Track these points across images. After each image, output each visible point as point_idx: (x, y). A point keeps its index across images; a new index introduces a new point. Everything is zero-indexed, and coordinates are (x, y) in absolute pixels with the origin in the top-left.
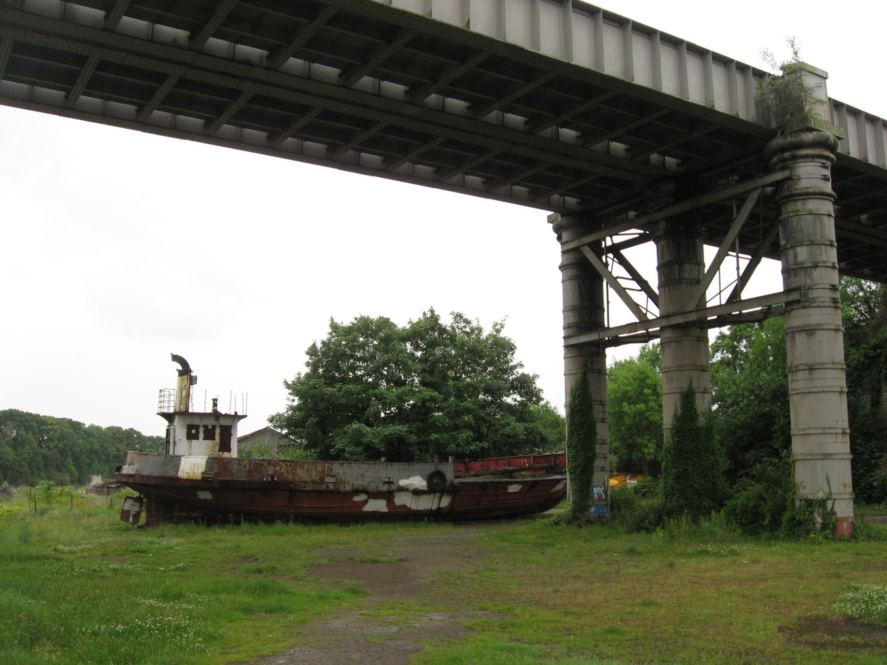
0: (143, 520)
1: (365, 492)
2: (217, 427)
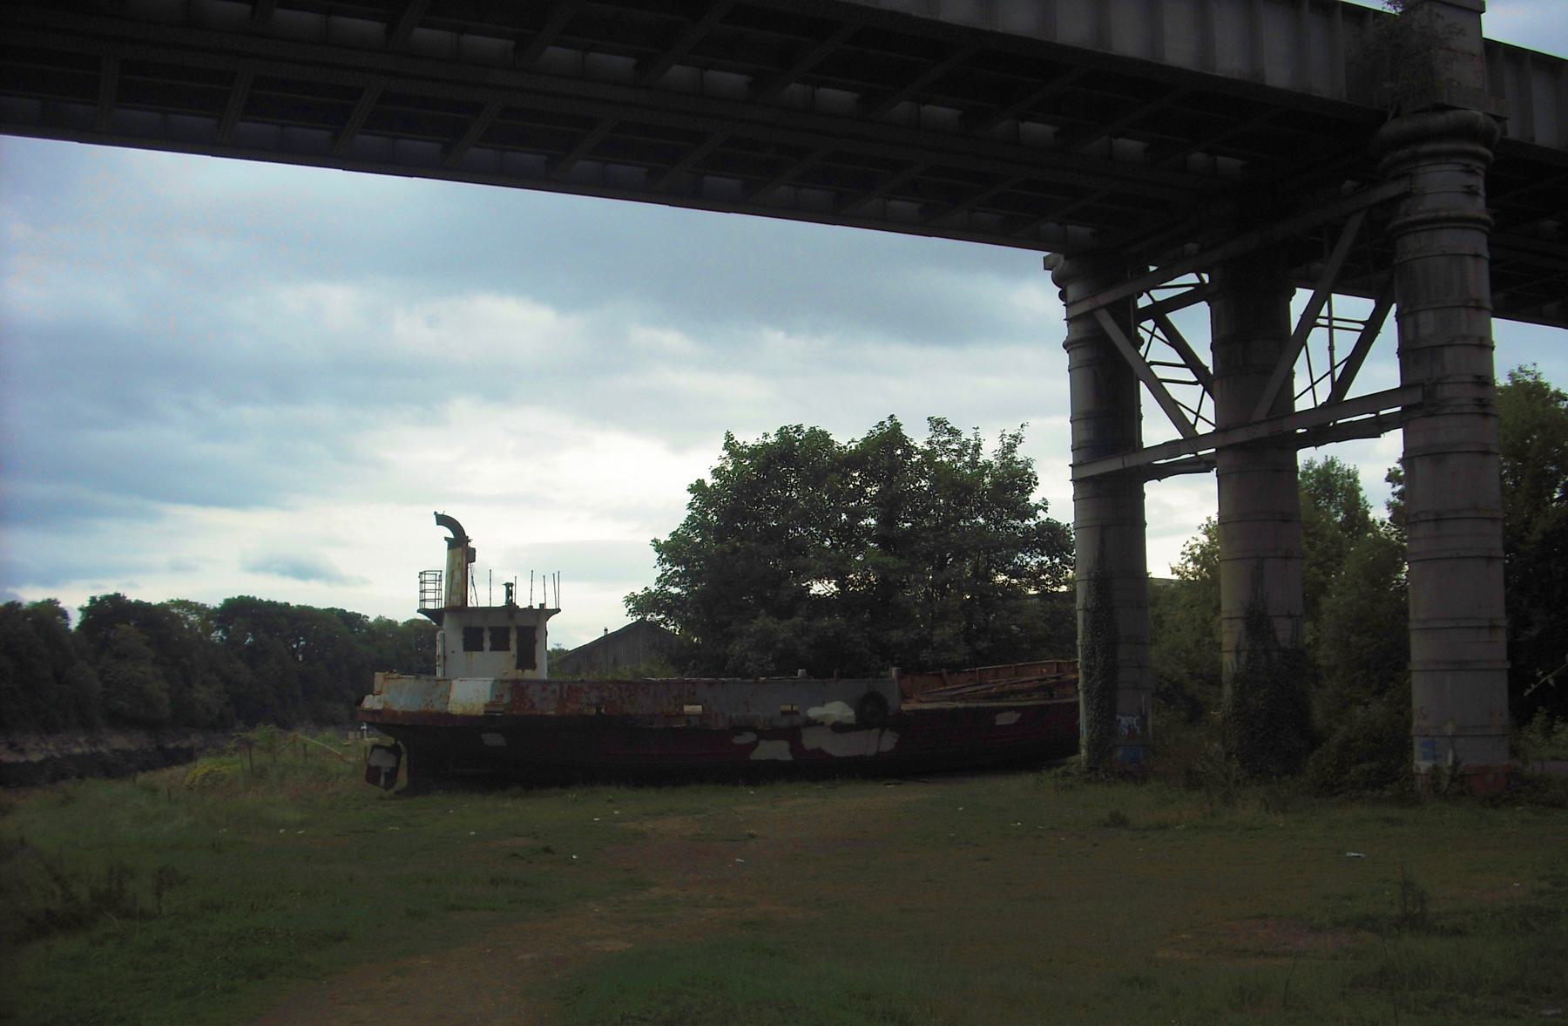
0: (403, 779)
1: (754, 730)
2: (518, 628)
